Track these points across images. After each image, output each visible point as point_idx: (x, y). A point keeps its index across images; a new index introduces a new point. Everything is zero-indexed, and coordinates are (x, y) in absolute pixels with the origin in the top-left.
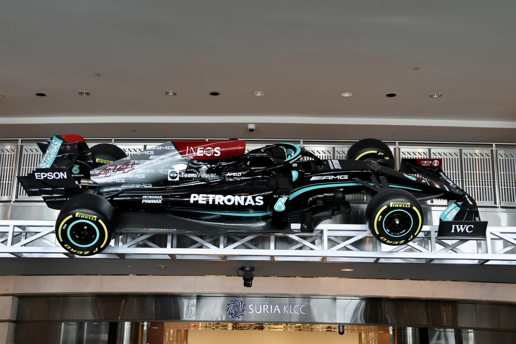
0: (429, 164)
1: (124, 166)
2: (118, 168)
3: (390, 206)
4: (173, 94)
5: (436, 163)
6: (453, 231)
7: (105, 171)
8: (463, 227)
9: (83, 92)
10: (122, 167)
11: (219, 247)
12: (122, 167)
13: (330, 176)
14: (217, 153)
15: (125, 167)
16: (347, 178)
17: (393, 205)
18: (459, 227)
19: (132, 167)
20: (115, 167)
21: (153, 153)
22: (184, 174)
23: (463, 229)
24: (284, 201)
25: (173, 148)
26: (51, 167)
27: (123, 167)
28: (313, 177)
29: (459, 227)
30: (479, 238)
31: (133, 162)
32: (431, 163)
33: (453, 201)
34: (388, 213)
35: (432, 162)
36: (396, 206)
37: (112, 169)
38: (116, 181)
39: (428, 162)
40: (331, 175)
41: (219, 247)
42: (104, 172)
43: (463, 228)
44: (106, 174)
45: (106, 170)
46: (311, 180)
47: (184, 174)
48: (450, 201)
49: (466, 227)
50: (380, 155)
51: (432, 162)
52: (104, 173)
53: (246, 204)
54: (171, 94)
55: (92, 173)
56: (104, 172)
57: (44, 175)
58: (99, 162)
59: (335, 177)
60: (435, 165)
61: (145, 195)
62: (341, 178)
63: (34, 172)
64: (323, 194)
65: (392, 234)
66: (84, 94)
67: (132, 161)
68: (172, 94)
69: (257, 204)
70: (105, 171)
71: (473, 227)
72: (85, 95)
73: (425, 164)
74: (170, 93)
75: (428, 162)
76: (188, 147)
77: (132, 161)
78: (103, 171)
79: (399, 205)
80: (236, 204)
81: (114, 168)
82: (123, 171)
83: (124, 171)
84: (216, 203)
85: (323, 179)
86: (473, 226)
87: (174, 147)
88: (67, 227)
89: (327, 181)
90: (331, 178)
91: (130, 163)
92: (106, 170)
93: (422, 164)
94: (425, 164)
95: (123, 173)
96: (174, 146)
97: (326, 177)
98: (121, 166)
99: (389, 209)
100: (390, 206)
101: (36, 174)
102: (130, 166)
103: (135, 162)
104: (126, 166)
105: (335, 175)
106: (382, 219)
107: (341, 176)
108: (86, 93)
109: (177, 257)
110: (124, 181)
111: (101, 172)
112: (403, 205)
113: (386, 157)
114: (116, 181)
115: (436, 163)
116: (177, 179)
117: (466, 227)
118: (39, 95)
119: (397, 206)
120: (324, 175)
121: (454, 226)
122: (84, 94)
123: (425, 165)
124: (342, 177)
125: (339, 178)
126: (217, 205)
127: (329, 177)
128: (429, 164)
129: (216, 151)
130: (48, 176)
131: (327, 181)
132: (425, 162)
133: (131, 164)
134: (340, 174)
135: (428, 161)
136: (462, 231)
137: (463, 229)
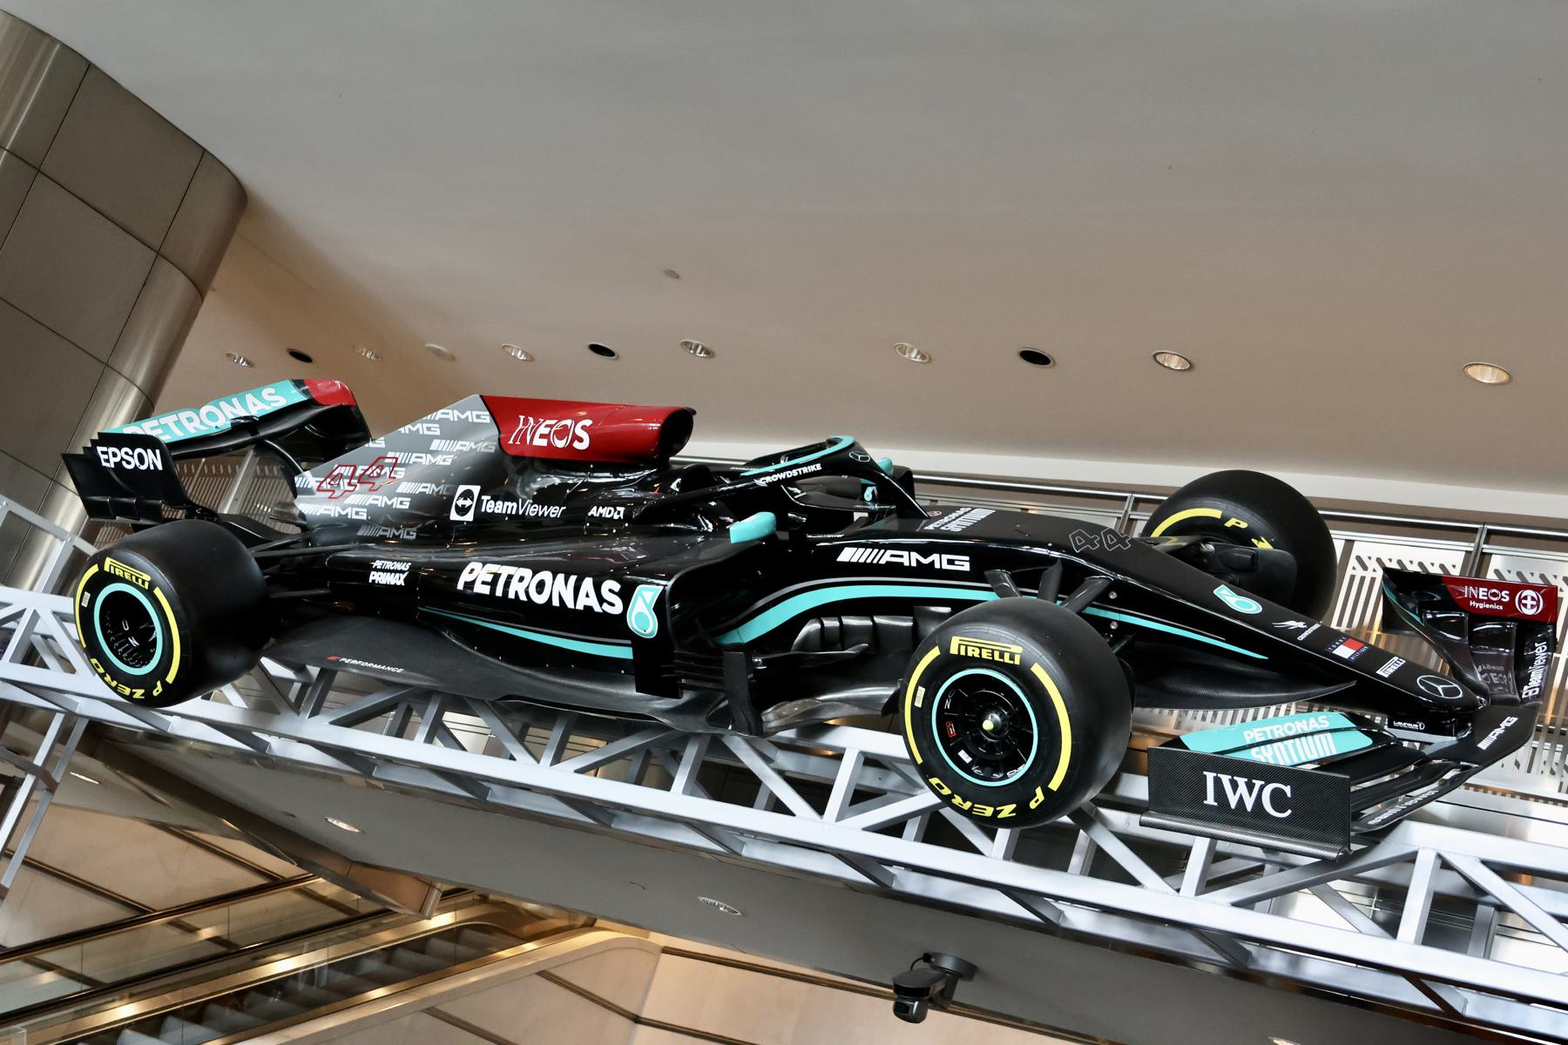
0: (1499, 603)
1: (374, 467)
2: (361, 475)
3: (951, 652)
4: (919, 356)
5: (1529, 602)
6: (1210, 800)
7: (332, 482)
8: (1250, 787)
9: (697, 346)
10: (368, 473)
11: (538, 761)
12: (368, 473)
13: (905, 554)
14: (581, 440)
15: (375, 474)
16: (966, 567)
17: (960, 645)
18: (1235, 786)
19: (392, 475)
20: (352, 468)
21: (438, 433)
22: (488, 501)
23: (1250, 795)
24: (654, 596)
25: (486, 418)
26: (167, 444)
27: (370, 470)
28: (846, 549)
29: (1235, 786)
30: (1308, 845)
31: (393, 458)
32: (1508, 599)
33: (1410, 725)
34: (1029, 700)
35: (1512, 597)
36: (970, 654)
37: (347, 477)
38: (347, 515)
39: (1495, 595)
40: (909, 548)
41: (538, 761)
42: (329, 483)
43: (1250, 790)
44: (334, 491)
45: (332, 477)
46: (839, 559)
47: (488, 501)
48: (1400, 724)
49: (1262, 788)
50: (1233, 526)
51: (1512, 597)
52: (329, 487)
53: (580, 607)
54: (914, 355)
55: (299, 482)
56: (329, 483)
57: (115, 455)
58: (963, 653)
59: (925, 558)
60: (1529, 612)
61: (380, 559)
62: (946, 566)
63: (95, 443)
64: (871, 617)
65: (998, 776)
66: (699, 351)
67: (390, 454)
68: (915, 358)
69: (606, 607)
70: (332, 482)
71: (1289, 795)
72: (700, 353)
73: (1481, 601)
74: (912, 350)
75: (1495, 595)
76: (522, 417)
77: (390, 454)
78: (325, 480)
79: (980, 648)
80: (556, 603)
81: (349, 474)
82: (370, 485)
83: (374, 484)
84: (511, 595)
85: (883, 562)
86: (1288, 790)
87: (488, 413)
88: (92, 602)
89: (894, 571)
90: (910, 559)
91: (387, 461)
92: (332, 477)
93: (1468, 599)
94: (1481, 601)
95: (370, 490)
96: (489, 410)
97: (892, 556)
98: (367, 467)
99: (949, 663)
100: (951, 652)
101: (100, 449)
102: (387, 470)
103: (397, 459)
104: (378, 470)
105: (925, 551)
106: (928, 700)
107: (945, 557)
108: (703, 349)
109: (493, 795)
110: (364, 517)
111: (322, 482)
112: (993, 650)
113: (1259, 540)
114: (347, 515)
115: (1529, 602)
116: (469, 517)
117: (1262, 788)
118: (597, 349)
119: (973, 652)
120: (887, 547)
121: (1210, 776)
122: (699, 351)
123: (1481, 606)
124: (951, 562)
125: (937, 566)
126: (511, 599)
127: (902, 556)
128: (1499, 603)
129: (580, 433)
130: (122, 459)
131: (894, 571)
132: (1482, 593)
133: (388, 465)
134: (942, 549)
135: (1494, 590)
136: (1249, 804)
137: (1250, 795)
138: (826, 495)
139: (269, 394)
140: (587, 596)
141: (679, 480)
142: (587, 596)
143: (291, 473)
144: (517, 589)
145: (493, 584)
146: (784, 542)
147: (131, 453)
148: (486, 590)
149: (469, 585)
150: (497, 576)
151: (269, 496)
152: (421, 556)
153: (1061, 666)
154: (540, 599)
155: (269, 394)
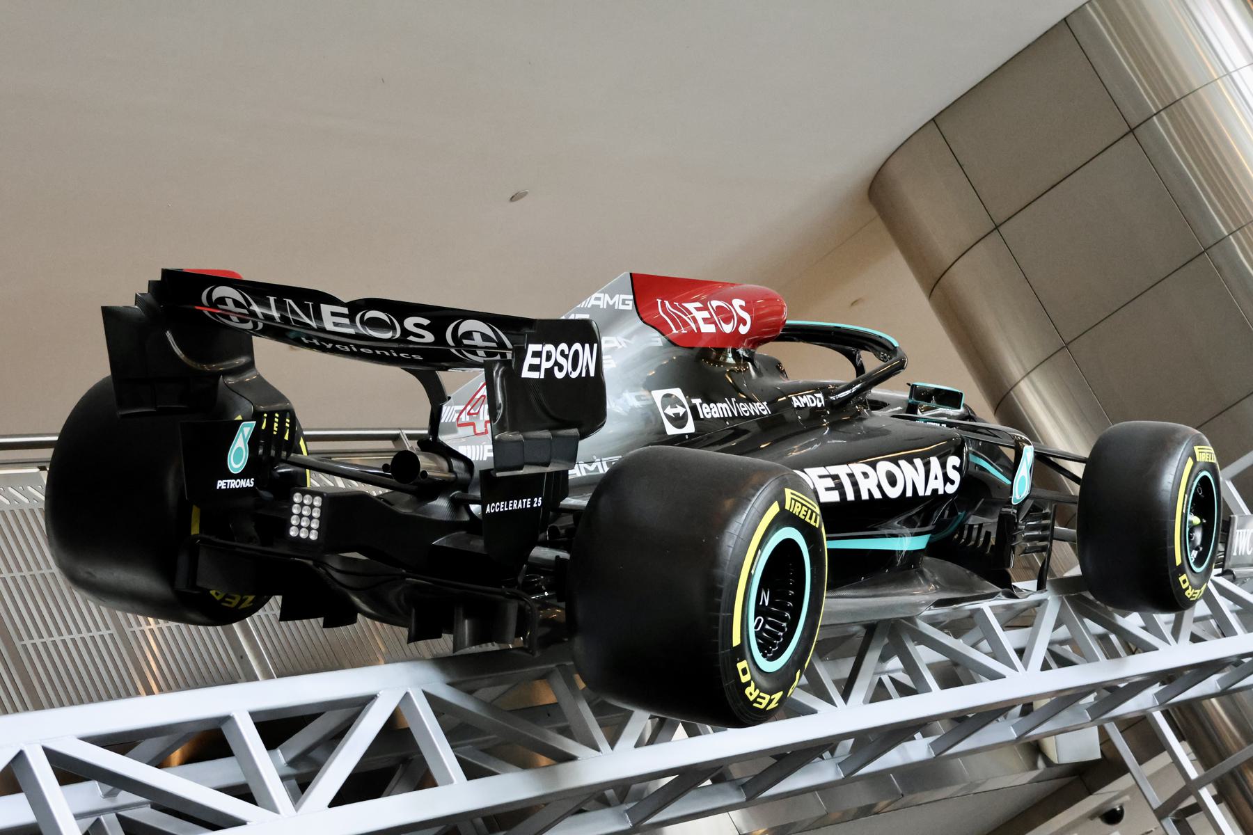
7: (472, 411)
78: (465, 409)
84: (865, 496)
111: (461, 412)
138: (1021, 718)
139: (821, 477)
140: (936, 478)
141: (564, 555)
142: (936, 478)
143: (623, 391)
144: (232, 486)
145: (226, 486)
146: (332, 346)
147: (556, 368)
148: (225, 487)
149: (220, 487)
150: (227, 483)
151: (280, 641)
152: (959, 521)
153: (1015, 405)
154: (893, 493)
155: (821, 477)
